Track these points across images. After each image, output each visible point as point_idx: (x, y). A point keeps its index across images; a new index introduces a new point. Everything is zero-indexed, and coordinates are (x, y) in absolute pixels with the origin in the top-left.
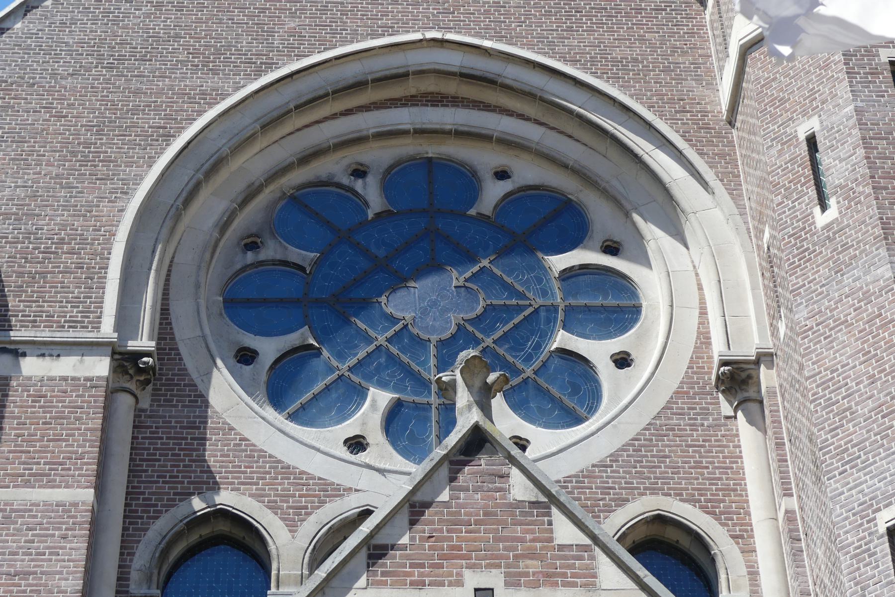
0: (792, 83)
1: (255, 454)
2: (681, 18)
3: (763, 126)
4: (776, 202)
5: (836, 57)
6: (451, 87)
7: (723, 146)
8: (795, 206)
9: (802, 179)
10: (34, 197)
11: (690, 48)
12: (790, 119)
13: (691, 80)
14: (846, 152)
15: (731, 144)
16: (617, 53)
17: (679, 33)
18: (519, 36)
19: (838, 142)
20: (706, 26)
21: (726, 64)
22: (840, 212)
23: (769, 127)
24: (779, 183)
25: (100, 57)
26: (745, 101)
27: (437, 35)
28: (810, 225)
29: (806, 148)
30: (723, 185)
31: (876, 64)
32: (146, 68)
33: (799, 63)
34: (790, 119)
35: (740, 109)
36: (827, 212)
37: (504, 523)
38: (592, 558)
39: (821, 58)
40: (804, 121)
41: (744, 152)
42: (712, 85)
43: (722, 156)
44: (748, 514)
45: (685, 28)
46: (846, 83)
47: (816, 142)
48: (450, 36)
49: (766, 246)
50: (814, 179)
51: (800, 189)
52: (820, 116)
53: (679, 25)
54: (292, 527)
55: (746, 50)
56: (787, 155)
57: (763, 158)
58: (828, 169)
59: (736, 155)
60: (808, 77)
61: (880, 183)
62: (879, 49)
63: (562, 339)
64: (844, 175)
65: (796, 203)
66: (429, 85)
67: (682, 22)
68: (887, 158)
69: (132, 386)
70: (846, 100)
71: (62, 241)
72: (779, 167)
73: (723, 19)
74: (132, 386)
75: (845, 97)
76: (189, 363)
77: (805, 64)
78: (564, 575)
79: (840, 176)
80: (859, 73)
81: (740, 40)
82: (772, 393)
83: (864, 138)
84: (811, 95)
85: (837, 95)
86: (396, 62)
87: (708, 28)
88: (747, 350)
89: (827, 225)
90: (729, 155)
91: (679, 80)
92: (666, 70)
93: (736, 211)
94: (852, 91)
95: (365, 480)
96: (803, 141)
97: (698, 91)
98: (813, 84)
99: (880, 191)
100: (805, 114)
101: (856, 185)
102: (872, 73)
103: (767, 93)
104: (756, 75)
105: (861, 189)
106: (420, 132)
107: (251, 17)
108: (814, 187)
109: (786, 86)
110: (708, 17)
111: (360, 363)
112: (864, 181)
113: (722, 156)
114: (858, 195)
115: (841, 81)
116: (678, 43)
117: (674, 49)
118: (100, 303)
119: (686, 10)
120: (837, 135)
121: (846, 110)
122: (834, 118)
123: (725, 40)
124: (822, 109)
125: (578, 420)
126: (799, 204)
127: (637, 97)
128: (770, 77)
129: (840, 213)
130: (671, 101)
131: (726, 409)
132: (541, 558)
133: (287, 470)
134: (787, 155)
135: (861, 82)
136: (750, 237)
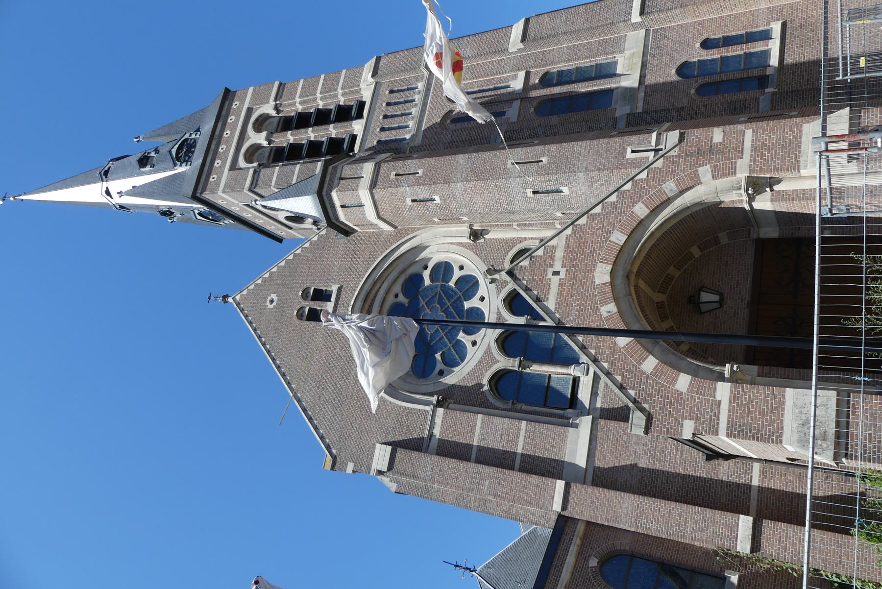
1: (473, 371)
10: (381, 429)
16: (367, 257)
18: (356, 284)
25: (338, 407)
27: (351, 307)
32: (344, 394)
36: (436, 199)
37: (535, 267)
38: (548, 246)
42: (381, 233)
43: (406, 231)
44: (514, 238)
48: (352, 304)
54: (498, 362)
55: (379, 217)
63: (452, 284)
69: (447, 404)
71: (398, 421)
74: (447, 404)
76: (442, 388)
78: (552, 253)
82: (481, 226)
88: (465, 229)
91: (379, 241)
92: (375, 244)
95: (486, 341)
107: (333, 361)
111: (449, 341)
113: (406, 231)
117: (369, 241)
118: (419, 410)
125: (477, 281)
127: (382, 253)
130: (386, 244)
131: (482, 240)
132: (546, 259)
133: (480, 362)
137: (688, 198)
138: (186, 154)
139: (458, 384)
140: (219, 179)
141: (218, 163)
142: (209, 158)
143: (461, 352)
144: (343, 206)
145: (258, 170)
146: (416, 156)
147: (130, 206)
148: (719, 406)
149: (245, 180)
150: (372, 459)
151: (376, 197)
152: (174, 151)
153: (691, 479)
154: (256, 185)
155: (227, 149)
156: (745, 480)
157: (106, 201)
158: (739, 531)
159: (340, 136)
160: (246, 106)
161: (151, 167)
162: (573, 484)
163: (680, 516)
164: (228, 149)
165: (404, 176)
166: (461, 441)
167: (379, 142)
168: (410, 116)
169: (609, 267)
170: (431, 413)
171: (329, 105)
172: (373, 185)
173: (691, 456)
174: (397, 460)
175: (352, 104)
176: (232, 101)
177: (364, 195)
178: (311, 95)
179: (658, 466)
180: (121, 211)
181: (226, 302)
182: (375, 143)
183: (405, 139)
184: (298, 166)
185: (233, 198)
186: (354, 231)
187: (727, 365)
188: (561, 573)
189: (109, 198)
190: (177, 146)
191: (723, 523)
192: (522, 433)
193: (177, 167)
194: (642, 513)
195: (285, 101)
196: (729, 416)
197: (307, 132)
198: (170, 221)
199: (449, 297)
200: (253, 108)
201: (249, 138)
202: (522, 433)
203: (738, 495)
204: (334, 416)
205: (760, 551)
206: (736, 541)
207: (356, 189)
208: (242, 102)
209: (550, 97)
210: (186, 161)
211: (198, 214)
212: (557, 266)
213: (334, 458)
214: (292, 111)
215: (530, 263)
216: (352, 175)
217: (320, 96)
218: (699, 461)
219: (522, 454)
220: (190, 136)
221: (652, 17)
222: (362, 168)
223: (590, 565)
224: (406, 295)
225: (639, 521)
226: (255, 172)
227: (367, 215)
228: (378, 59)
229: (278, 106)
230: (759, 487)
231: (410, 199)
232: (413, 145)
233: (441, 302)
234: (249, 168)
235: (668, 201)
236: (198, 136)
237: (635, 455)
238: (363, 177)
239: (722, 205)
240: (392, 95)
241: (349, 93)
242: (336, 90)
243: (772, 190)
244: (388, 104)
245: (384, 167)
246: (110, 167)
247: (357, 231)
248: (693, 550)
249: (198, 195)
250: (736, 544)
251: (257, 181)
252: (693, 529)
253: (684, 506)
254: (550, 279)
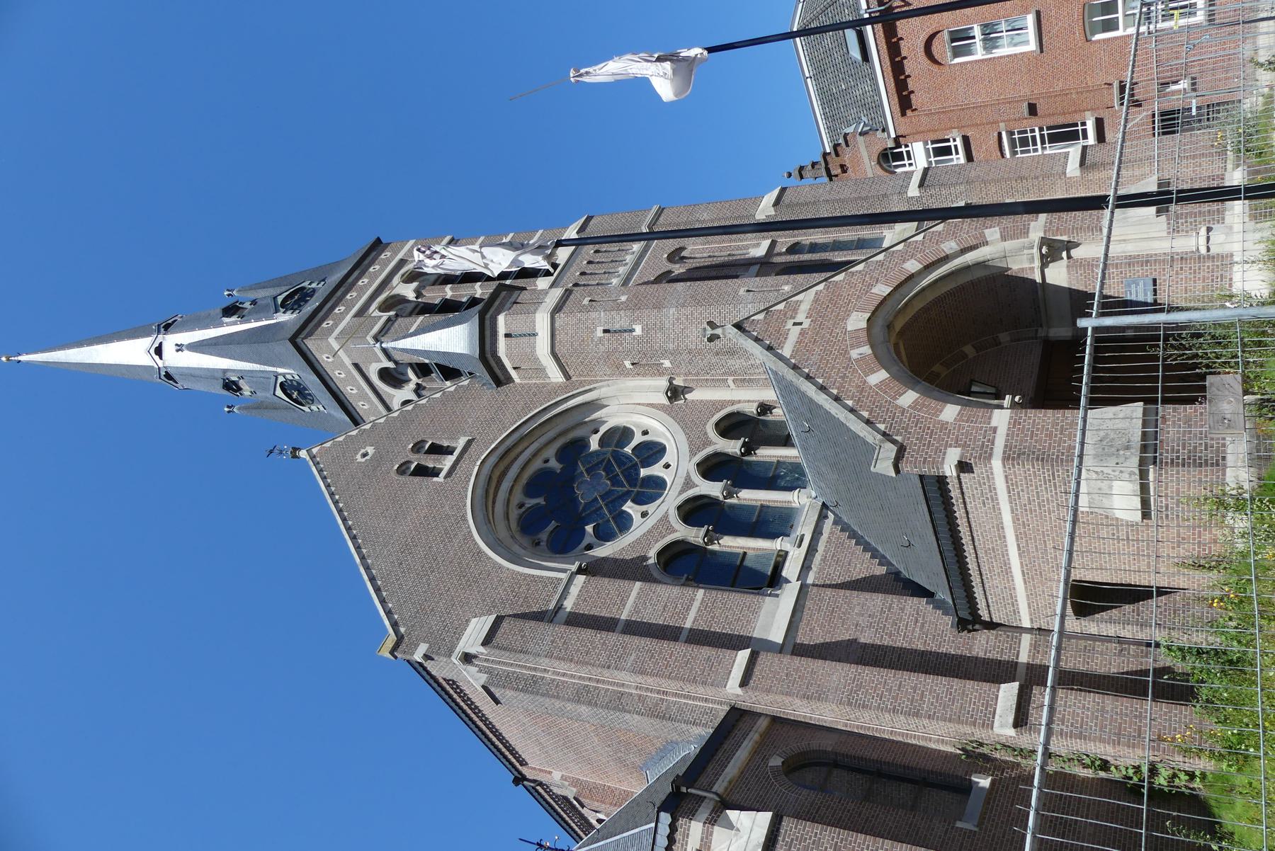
1: (638, 541)
6: (501, 467)
16: (519, 409)
27: (480, 461)
48: (483, 458)
66: (497, 473)
86: (483, 477)
88: (663, 383)
92: (535, 396)
106: (515, 481)
137: (970, 257)
138: (297, 302)
139: (612, 556)
141: (340, 309)
142: (329, 305)
143: (624, 523)
148: (995, 432)
150: (458, 639)
151: (557, 325)
152: (280, 299)
153: (933, 656)
154: (386, 333)
155: (367, 284)
156: (1009, 656)
157: (151, 363)
158: (998, 704)
162: (762, 653)
163: (915, 689)
164: (370, 284)
166: (602, 614)
169: (867, 315)
170: (565, 582)
172: (558, 309)
173: (936, 629)
174: (501, 631)
177: (542, 321)
179: (887, 641)
181: (295, 456)
187: (1007, 396)
188: (726, 766)
189: (157, 358)
191: (976, 696)
192: (696, 604)
194: (860, 686)
196: (1007, 441)
199: (620, 464)
200: (407, 261)
202: (696, 604)
203: (998, 675)
204: (416, 586)
205: (1026, 725)
206: (994, 718)
209: (797, 264)
212: (800, 317)
213: (400, 639)
215: (765, 317)
218: (946, 635)
219: (691, 629)
220: (310, 284)
221: (933, 191)
223: (769, 765)
224: (559, 459)
225: (854, 697)
230: (1028, 664)
233: (608, 469)
235: (946, 259)
236: (320, 286)
237: (856, 628)
239: (1009, 273)
240: (597, 255)
243: (1069, 257)
248: (926, 753)
249: (299, 340)
250: (993, 722)
251: (389, 329)
252: (932, 705)
253: (922, 677)
254: (789, 330)
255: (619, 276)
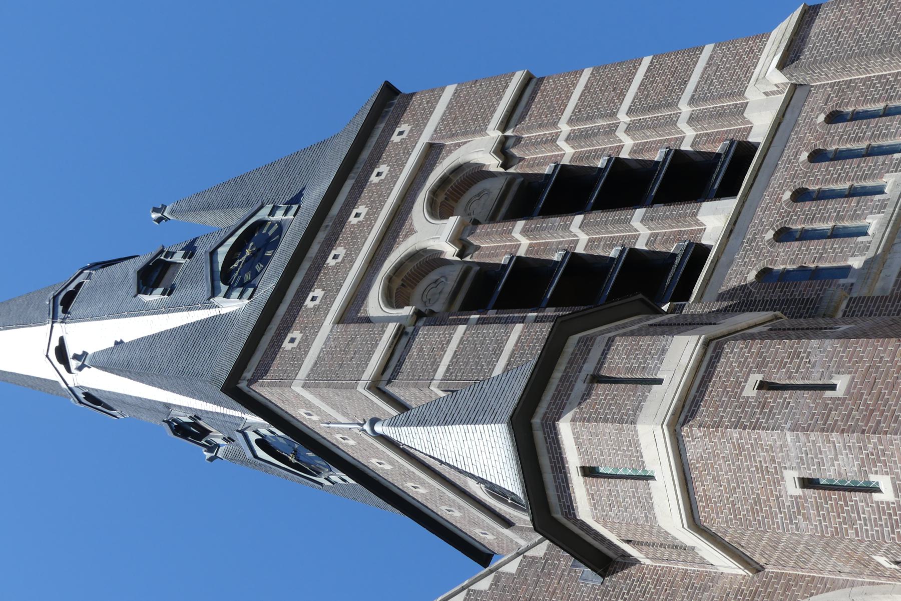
0: (743, 487)
2: (639, 587)
3: (774, 528)
4: (854, 536)
5: (735, 435)
7: (778, 584)
8: (865, 518)
9: (840, 503)
11: (671, 587)
12: (778, 499)
13: (702, 595)
14: (830, 451)
15: (778, 576)
17: (652, 593)
19: (817, 457)
20: (656, 566)
21: (701, 554)
22: (887, 473)
23: (778, 523)
24: (836, 528)
26: (743, 543)
28: (889, 509)
29: (812, 490)
30: (817, 594)
31: (756, 401)
33: (726, 474)
34: (778, 499)
35: (748, 554)
36: (882, 487)
39: (730, 450)
40: (784, 485)
41: (792, 564)
42: (715, 578)
43: (787, 587)
45: (650, 586)
46: (763, 433)
47: (808, 479)
49: (894, 566)
50: (845, 491)
51: (849, 508)
52: (785, 468)
53: (645, 591)
55: (695, 524)
56: (812, 512)
57: (806, 538)
58: (840, 474)
59: (792, 574)
60: (743, 469)
61: (871, 427)
62: (743, 395)
64: (851, 459)
65: (862, 516)
67: (643, 587)
68: (850, 414)
70: (779, 437)
72: (821, 523)
73: (656, 541)
75: (776, 437)
77: (730, 469)
79: (851, 464)
80: (759, 419)
81: (683, 527)
83: (823, 430)
84: (762, 470)
85: (771, 445)
87: (658, 565)
89: (894, 491)
90: (789, 580)
93: (848, 590)
94: (773, 430)
96: (803, 491)
97: (716, 592)
98: (752, 466)
99: (879, 428)
100: (778, 482)
101: (865, 450)
102: (763, 408)
103: (744, 515)
104: (723, 521)
105: (870, 446)
108: (853, 493)
109: (744, 494)
110: (648, 562)
112: (864, 441)
113: (787, 587)
114: (876, 451)
115: (760, 437)
116: (662, 597)
119: (634, 580)
120: (810, 456)
121: (789, 440)
122: (792, 454)
123: (677, 547)
124: (779, 463)
126: (864, 513)
128: (729, 508)
129: (888, 474)
134: (812, 512)
135: (768, 419)
136: (878, 584)
140: (306, 343)
144: (589, 472)
145: (410, 329)
146: (844, 327)
147: (108, 399)
149: (370, 353)
151: (692, 452)
154: (394, 376)
157: (55, 377)
159: (600, 252)
160: (425, 138)
161: (163, 294)
164: (350, 260)
165: (786, 394)
167: (765, 274)
168: (877, 197)
171: (649, 150)
175: (718, 150)
176: (396, 123)
178: (602, 116)
180: (89, 411)
182: (752, 276)
183: (846, 271)
184: (519, 327)
185: (334, 406)
186: (627, 561)
189: (61, 368)
190: (232, 240)
193: (218, 300)
195: (529, 129)
197: (566, 228)
198: (208, 455)
200: (441, 147)
201: (412, 231)
207: (630, 418)
208: (418, 129)
210: (244, 285)
211: (257, 441)
214: (544, 162)
216: (628, 370)
217: (627, 119)
220: (272, 213)
222: (664, 351)
226: (401, 333)
227: (657, 511)
228: (809, 15)
229: (510, 142)
231: (795, 474)
232: (864, 292)
234: (390, 320)
236: (290, 216)
238: (660, 382)
241: (711, 116)
242: (673, 104)
244: (817, 156)
245: (734, 352)
246: (80, 284)
247: (636, 562)
249: (243, 385)
251: (400, 363)
255: (883, 206)
